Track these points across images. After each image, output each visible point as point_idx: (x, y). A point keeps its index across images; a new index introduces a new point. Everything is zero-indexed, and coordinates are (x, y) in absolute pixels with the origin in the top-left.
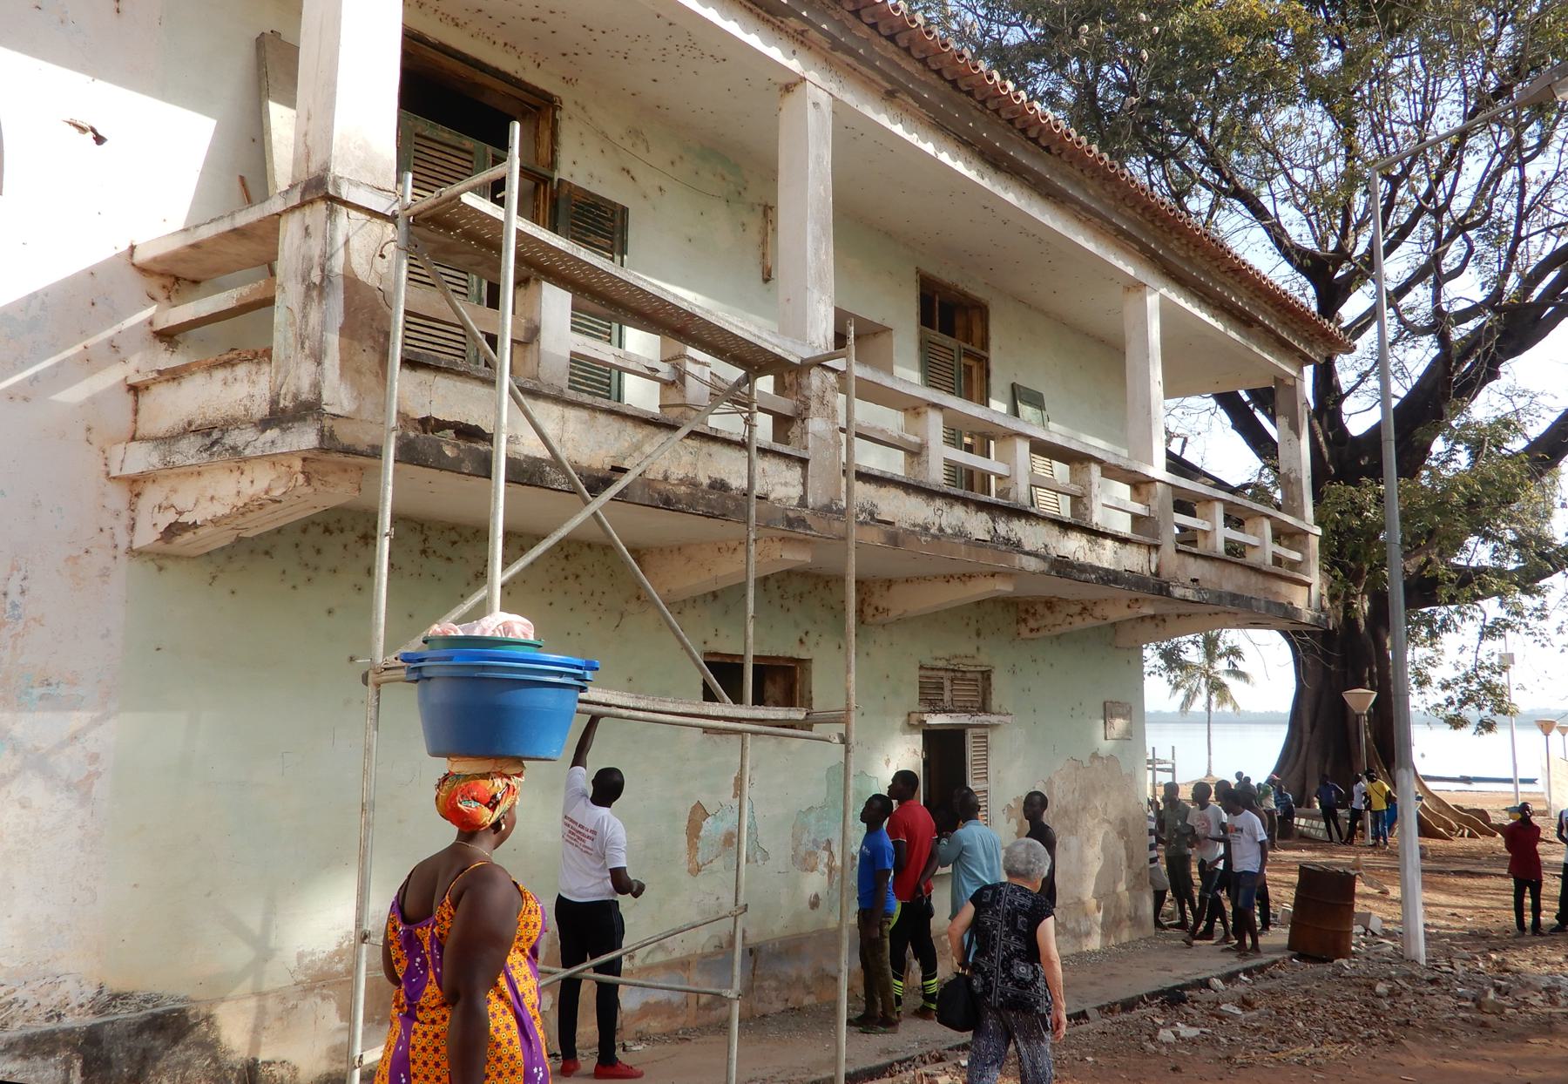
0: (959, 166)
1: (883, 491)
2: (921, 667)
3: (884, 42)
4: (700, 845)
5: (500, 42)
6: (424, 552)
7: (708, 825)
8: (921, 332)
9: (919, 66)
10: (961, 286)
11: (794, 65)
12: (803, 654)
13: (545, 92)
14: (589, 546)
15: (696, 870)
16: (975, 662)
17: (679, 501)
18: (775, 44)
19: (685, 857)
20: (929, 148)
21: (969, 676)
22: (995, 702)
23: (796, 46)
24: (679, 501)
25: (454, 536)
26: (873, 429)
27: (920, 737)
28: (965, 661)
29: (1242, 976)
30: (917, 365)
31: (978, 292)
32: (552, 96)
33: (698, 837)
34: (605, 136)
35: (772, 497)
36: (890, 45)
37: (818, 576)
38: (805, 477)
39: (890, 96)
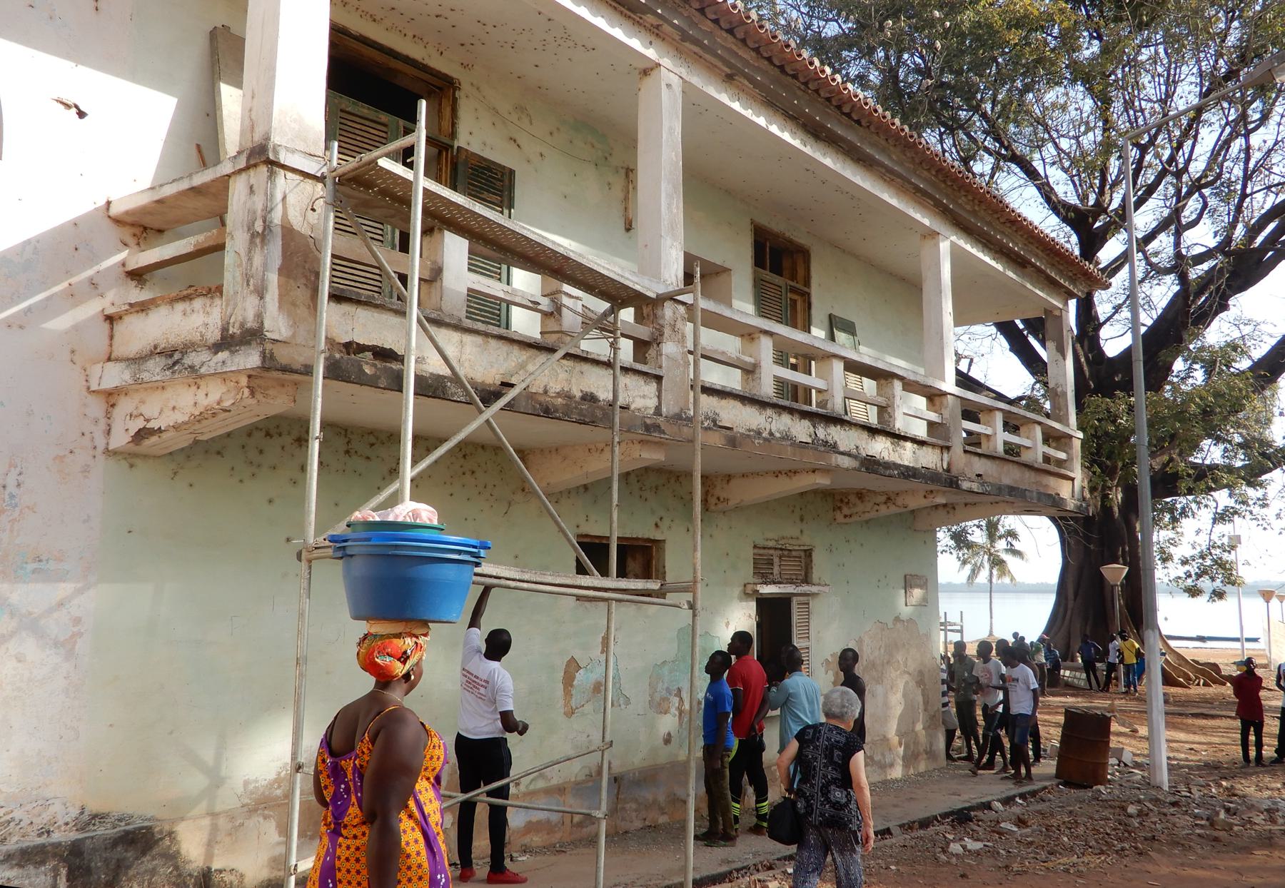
0: (786, 136)
1: (724, 402)
2: (755, 547)
3: (725, 34)
4: (573, 692)
5: (410, 34)
6: (347, 452)
7: (580, 676)
8: (755, 272)
9: (753, 54)
10: (787, 234)
11: (651, 53)
12: (658, 536)
13: (446, 75)
14: (483, 447)
15: (570, 713)
16: (799, 542)
17: (556, 411)
18: (635, 36)
19: (562, 702)
20: (761, 121)
21: (794, 553)
22: (816, 575)
23: (653, 38)
24: (556, 411)
25: (372, 439)
26: (716, 351)
27: (754, 604)
28: (791, 541)
29: (1017, 799)
30: (751, 299)
31: (802, 239)
32: (452, 79)
33: (572, 686)
34: (496, 112)
35: (632, 407)
36: (729, 37)
37: (671, 472)
38: (659, 391)
39: (729, 79)
